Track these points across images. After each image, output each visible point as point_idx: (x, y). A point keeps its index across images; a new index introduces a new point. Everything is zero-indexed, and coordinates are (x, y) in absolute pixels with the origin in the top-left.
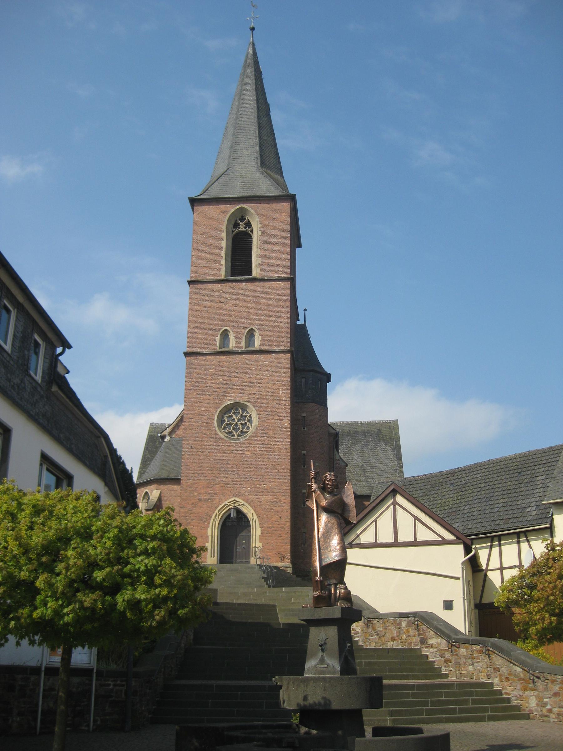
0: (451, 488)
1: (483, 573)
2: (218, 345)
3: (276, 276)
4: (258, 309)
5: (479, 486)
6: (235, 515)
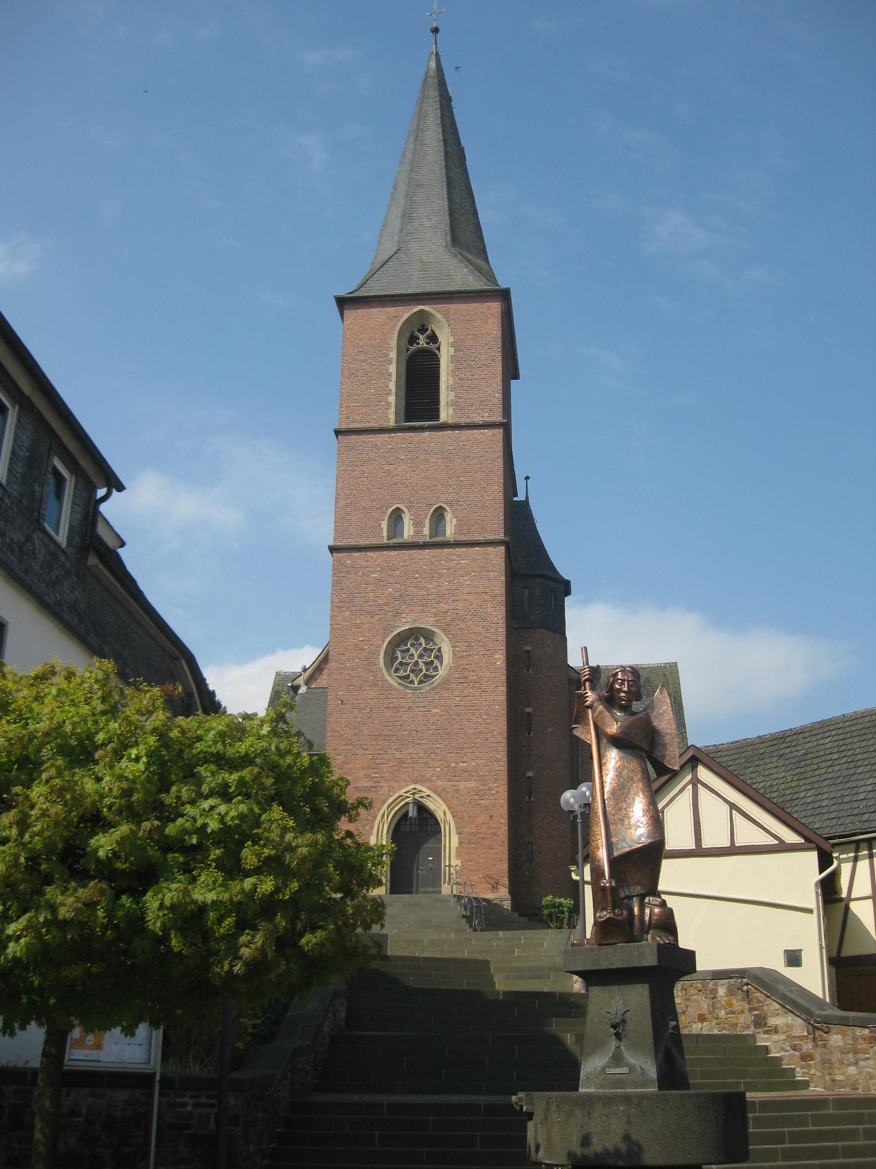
0: (781, 762)
1: (843, 904)
2: (385, 534)
3: (479, 420)
4: (448, 472)
5: (829, 757)
6: (415, 814)
